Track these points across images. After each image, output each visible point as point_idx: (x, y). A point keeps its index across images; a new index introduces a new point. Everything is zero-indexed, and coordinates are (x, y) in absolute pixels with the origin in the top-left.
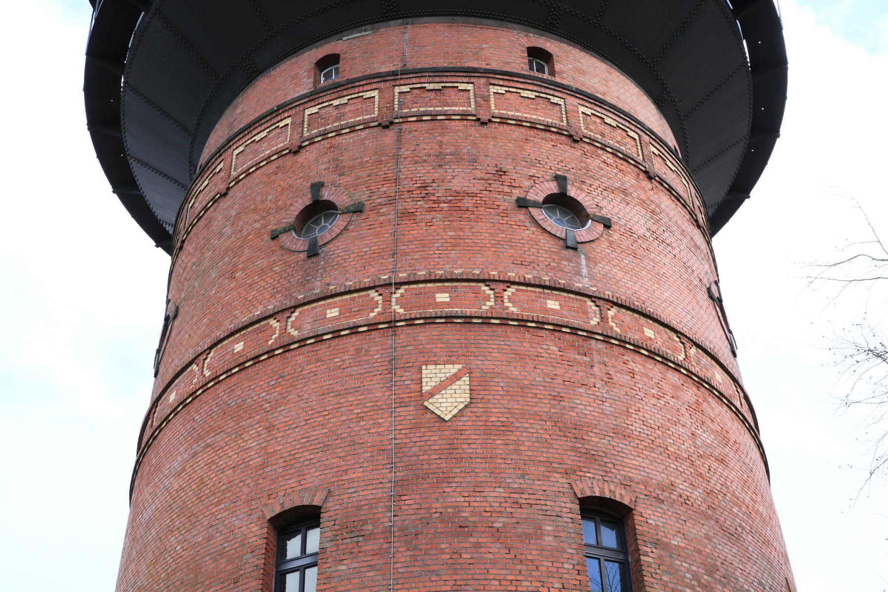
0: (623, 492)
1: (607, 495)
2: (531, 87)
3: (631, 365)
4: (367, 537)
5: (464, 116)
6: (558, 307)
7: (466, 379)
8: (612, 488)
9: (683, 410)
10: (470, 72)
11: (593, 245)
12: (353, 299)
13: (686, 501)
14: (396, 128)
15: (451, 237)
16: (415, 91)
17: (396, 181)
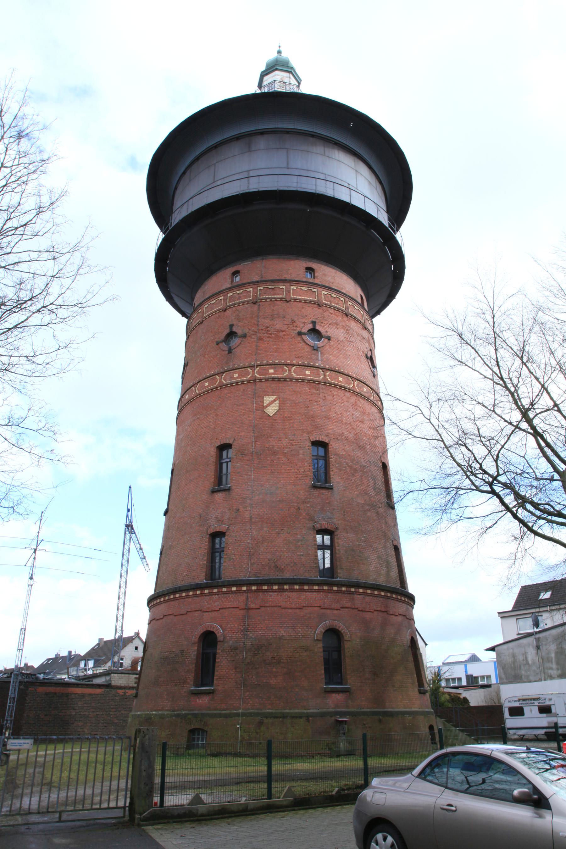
0: (326, 438)
1: (321, 440)
2: (305, 286)
3: (333, 392)
4: (246, 455)
5: (281, 299)
6: (309, 373)
7: (278, 401)
8: (323, 437)
9: (350, 406)
10: (284, 281)
11: (323, 348)
12: (242, 371)
13: (347, 438)
14: (258, 304)
15: (275, 348)
16: (265, 289)
17: (258, 325)
